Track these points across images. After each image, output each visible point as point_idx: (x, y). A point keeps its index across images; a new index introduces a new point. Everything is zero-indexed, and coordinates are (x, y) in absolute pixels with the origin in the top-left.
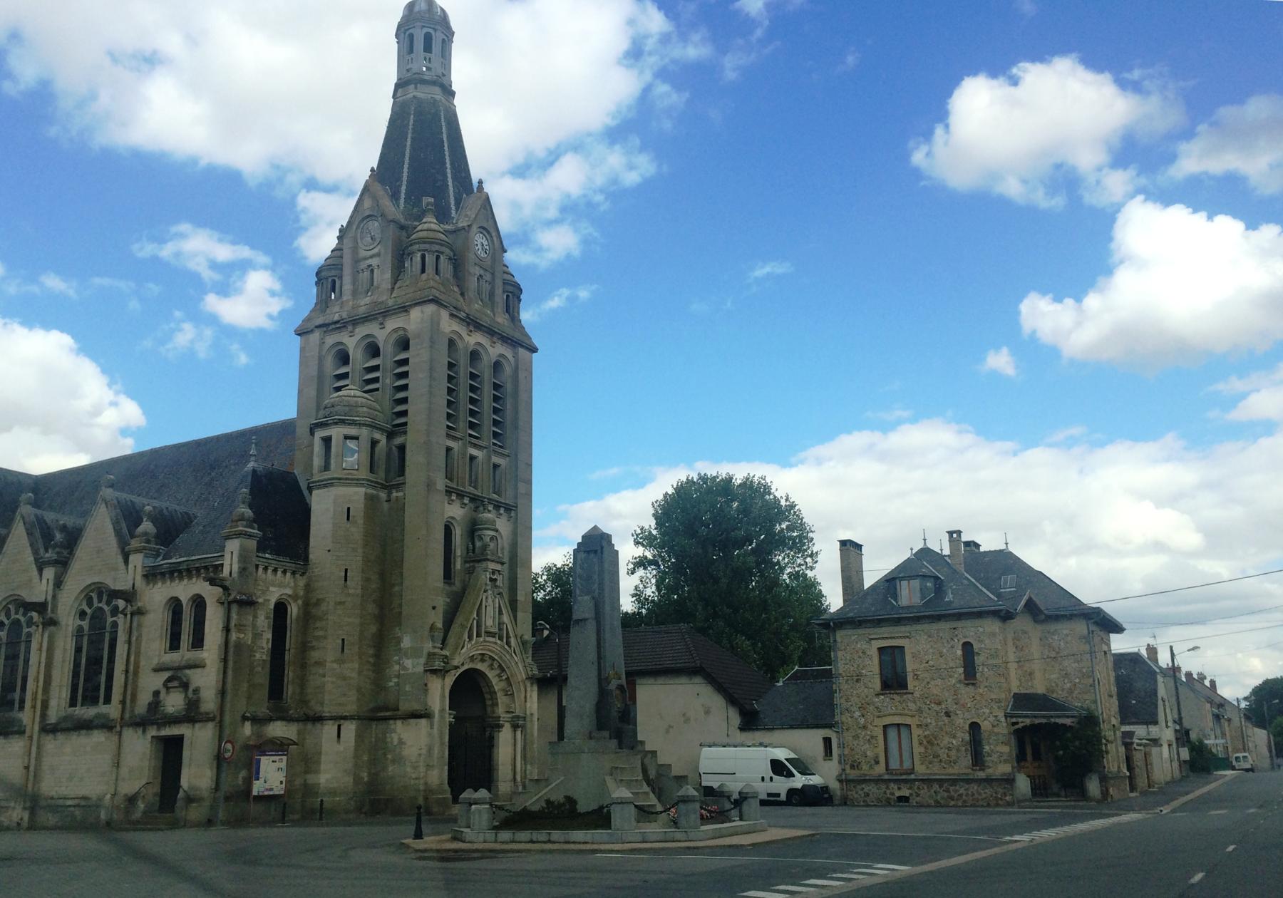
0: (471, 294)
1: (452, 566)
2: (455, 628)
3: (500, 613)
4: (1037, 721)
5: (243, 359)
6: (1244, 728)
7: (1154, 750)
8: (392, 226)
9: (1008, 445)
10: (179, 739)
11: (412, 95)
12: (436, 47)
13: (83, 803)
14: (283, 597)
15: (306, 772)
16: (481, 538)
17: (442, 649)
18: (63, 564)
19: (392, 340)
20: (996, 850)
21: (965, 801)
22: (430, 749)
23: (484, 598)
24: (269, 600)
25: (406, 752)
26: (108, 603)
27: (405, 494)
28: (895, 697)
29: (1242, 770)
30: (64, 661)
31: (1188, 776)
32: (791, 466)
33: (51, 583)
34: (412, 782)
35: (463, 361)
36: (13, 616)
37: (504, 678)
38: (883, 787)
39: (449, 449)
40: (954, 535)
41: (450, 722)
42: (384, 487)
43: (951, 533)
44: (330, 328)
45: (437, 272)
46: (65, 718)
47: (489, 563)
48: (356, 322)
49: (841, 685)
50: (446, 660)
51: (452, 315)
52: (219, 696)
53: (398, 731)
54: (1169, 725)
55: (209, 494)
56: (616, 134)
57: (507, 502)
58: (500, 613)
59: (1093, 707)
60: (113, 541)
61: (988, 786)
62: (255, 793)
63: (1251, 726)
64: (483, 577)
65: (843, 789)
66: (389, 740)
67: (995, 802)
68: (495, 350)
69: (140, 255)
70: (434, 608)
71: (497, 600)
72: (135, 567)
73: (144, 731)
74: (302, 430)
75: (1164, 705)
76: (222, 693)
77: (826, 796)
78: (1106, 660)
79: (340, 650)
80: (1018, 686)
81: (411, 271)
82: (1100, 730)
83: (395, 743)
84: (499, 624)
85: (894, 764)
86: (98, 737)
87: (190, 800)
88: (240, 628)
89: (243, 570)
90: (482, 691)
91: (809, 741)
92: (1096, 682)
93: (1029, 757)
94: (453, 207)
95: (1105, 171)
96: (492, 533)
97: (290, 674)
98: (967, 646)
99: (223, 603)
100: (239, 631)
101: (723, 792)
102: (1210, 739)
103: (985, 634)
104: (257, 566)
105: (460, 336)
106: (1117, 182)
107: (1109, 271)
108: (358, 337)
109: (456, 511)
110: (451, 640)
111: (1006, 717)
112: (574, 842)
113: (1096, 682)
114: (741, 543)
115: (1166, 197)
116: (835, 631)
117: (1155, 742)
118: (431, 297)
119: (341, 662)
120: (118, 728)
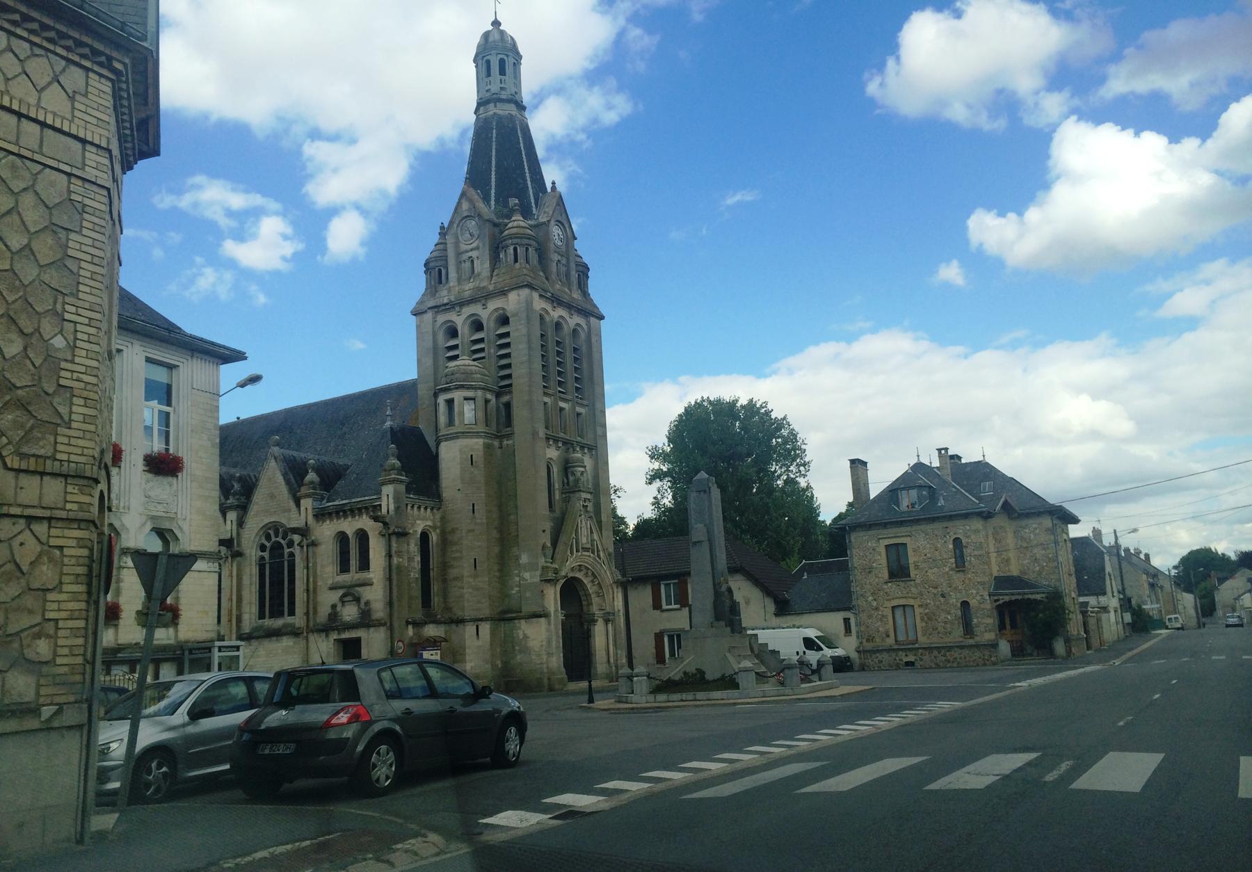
0: (554, 277)
2: (560, 547)
3: (592, 532)
4: (1013, 598)
5: (262, 299)
6: (1174, 594)
7: (1104, 616)
8: (487, 224)
9: (960, 349)
10: (357, 641)
11: (493, 111)
14: (427, 528)
16: (573, 474)
17: (552, 563)
18: (243, 508)
19: (493, 318)
20: (1008, 692)
21: (958, 663)
22: (549, 641)
24: (416, 531)
25: (531, 644)
26: (284, 538)
27: (514, 442)
28: (901, 583)
29: (1174, 629)
30: (251, 584)
31: (1131, 635)
32: (766, 376)
33: (235, 523)
34: (538, 666)
35: (550, 332)
37: (596, 583)
38: (894, 655)
40: (942, 452)
41: (562, 620)
42: (497, 437)
43: (939, 450)
44: (441, 309)
45: (527, 262)
46: (255, 629)
47: (582, 493)
48: (462, 303)
49: (857, 576)
50: (556, 571)
51: (541, 296)
52: (388, 606)
53: (522, 627)
54: (1115, 594)
55: (344, 445)
56: (596, 75)
57: (589, 443)
58: (592, 532)
59: (1058, 584)
60: (284, 489)
61: (977, 650)
63: (1179, 591)
65: (861, 658)
67: (983, 662)
68: (574, 320)
69: (161, 206)
70: (544, 531)
72: (306, 509)
74: (424, 392)
75: (1111, 579)
76: (390, 604)
77: (848, 664)
78: (1066, 546)
80: (998, 571)
81: (506, 261)
82: (1064, 602)
83: (521, 637)
84: (591, 540)
85: (901, 637)
88: (399, 554)
89: (397, 509)
90: (577, 590)
91: (834, 622)
92: (1060, 565)
93: (1008, 627)
94: (534, 206)
95: (1042, 94)
96: (582, 469)
97: (435, 587)
98: (957, 542)
99: (384, 535)
100: (399, 556)
101: (803, 662)
102: (1147, 605)
103: (973, 533)
104: (407, 505)
105: (547, 312)
106: (1053, 104)
107: (1046, 186)
108: (464, 316)
109: (553, 453)
110: (557, 556)
111: (990, 595)
112: (714, 700)
113: (1060, 565)
114: (741, 457)
115: (1096, 116)
116: (850, 534)
117: (1105, 609)
118: (525, 283)
119: (476, 576)
120: (305, 634)
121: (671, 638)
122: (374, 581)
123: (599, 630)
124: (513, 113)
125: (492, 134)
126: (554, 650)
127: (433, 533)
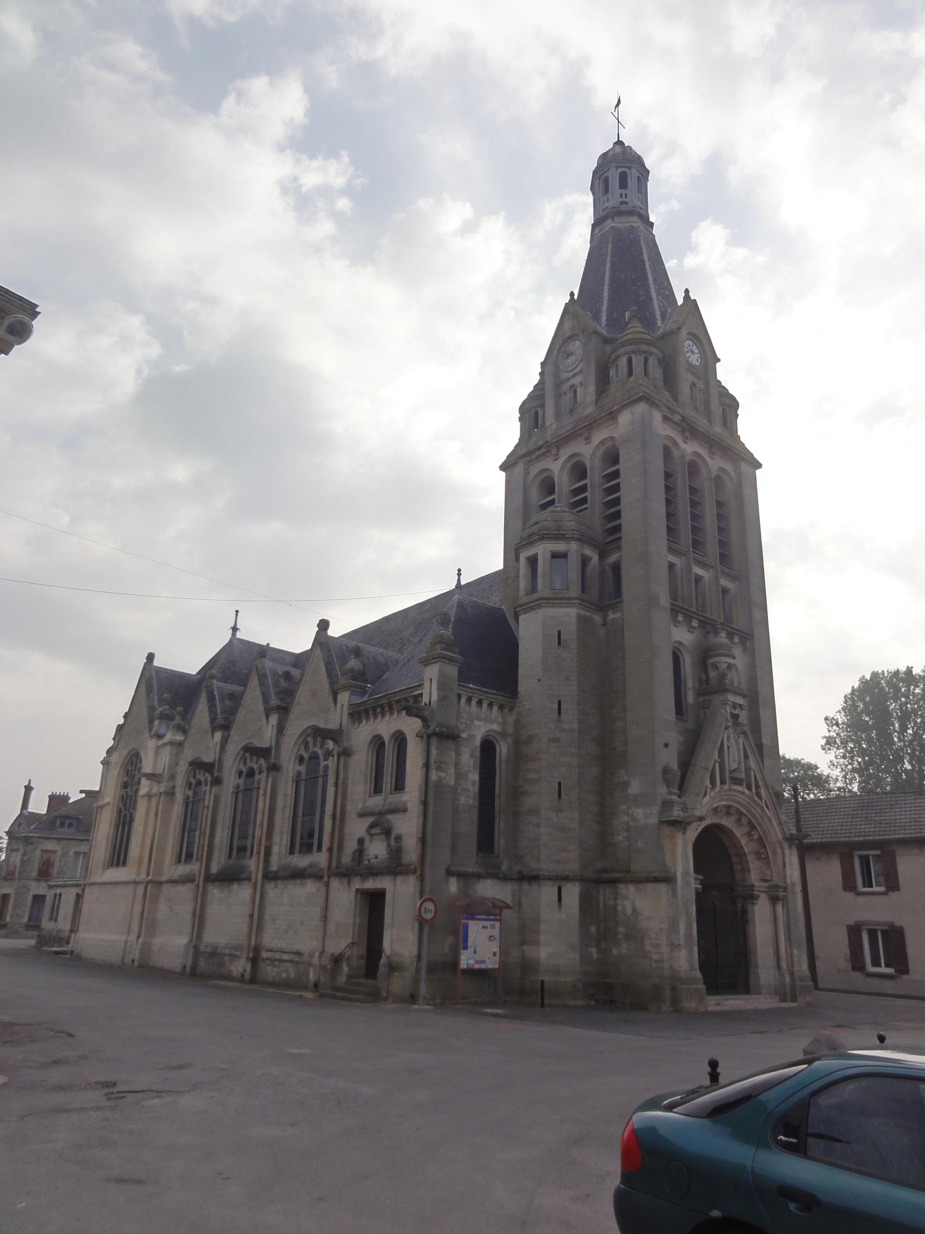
1: (683, 701)
3: (746, 757)
12: (632, 182)
13: (296, 959)
15: (524, 942)
16: (715, 667)
19: (600, 453)
23: (725, 736)
24: (473, 737)
30: (284, 807)
36: (249, 764)
37: (756, 837)
39: (671, 566)
44: (534, 456)
51: (665, 418)
58: (746, 757)
62: (463, 965)
64: (723, 711)
66: (619, 908)
68: (715, 463)
70: (666, 745)
71: (741, 740)
72: (343, 705)
73: (349, 883)
76: (423, 841)
79: (557, 796)
86: (310, 887)
87: (393, 967)
89: (442, 699)
97: (501, 824)
99: (422, 737)
100: (439, 769)
104: (459, 696)
105: (676, 444)
108: (562, 459)
109: (684, 636)
118: (640, 394)
120: (326, 879)
121: (872, 934)
122: (409, 805)
123: (761, 911)
124: (636, 225)
125: (607, 249)
126: (682, 942)
127: (501, 743)
